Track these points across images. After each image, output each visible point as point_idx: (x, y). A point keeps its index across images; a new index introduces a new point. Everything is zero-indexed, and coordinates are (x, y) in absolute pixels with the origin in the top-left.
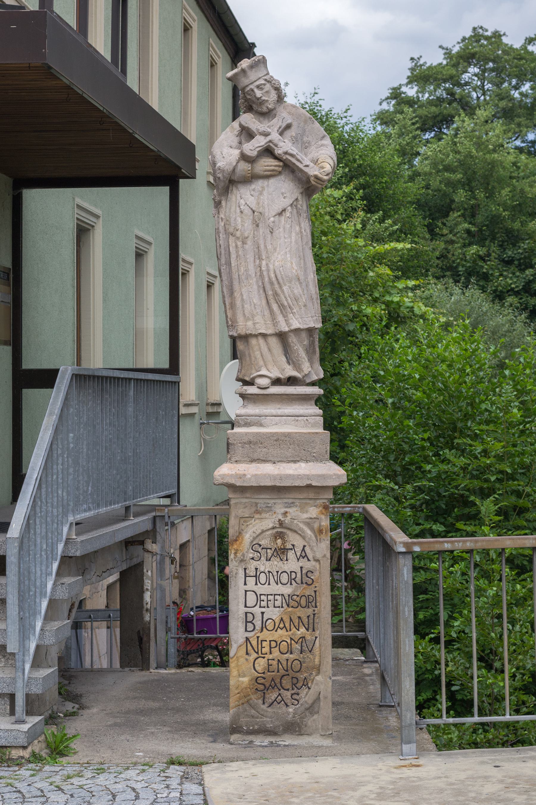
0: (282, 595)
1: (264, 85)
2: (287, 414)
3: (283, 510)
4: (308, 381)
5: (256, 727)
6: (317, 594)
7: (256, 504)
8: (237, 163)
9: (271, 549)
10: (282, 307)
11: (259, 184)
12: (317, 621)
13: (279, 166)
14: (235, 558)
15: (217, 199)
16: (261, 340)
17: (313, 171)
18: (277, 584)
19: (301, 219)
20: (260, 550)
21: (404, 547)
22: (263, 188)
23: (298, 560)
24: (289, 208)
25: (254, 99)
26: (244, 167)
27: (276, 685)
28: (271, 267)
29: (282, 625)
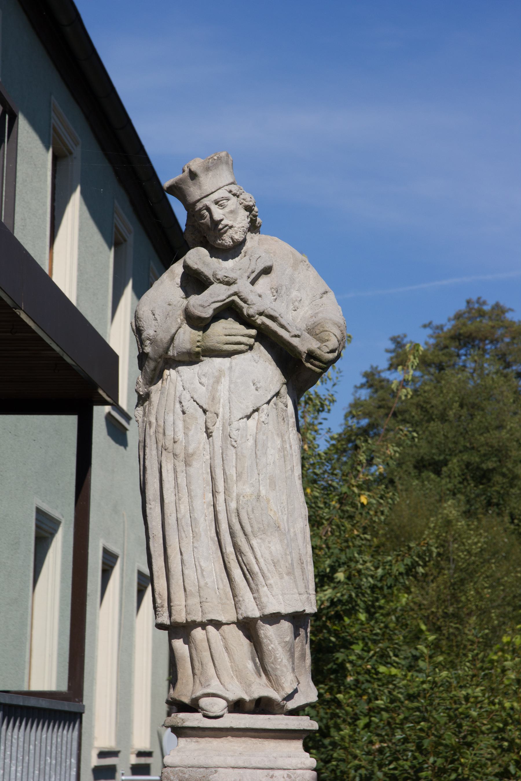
2: (254, 765)
4: (291, 705)
13: (250, 336)
26: (187, 338)
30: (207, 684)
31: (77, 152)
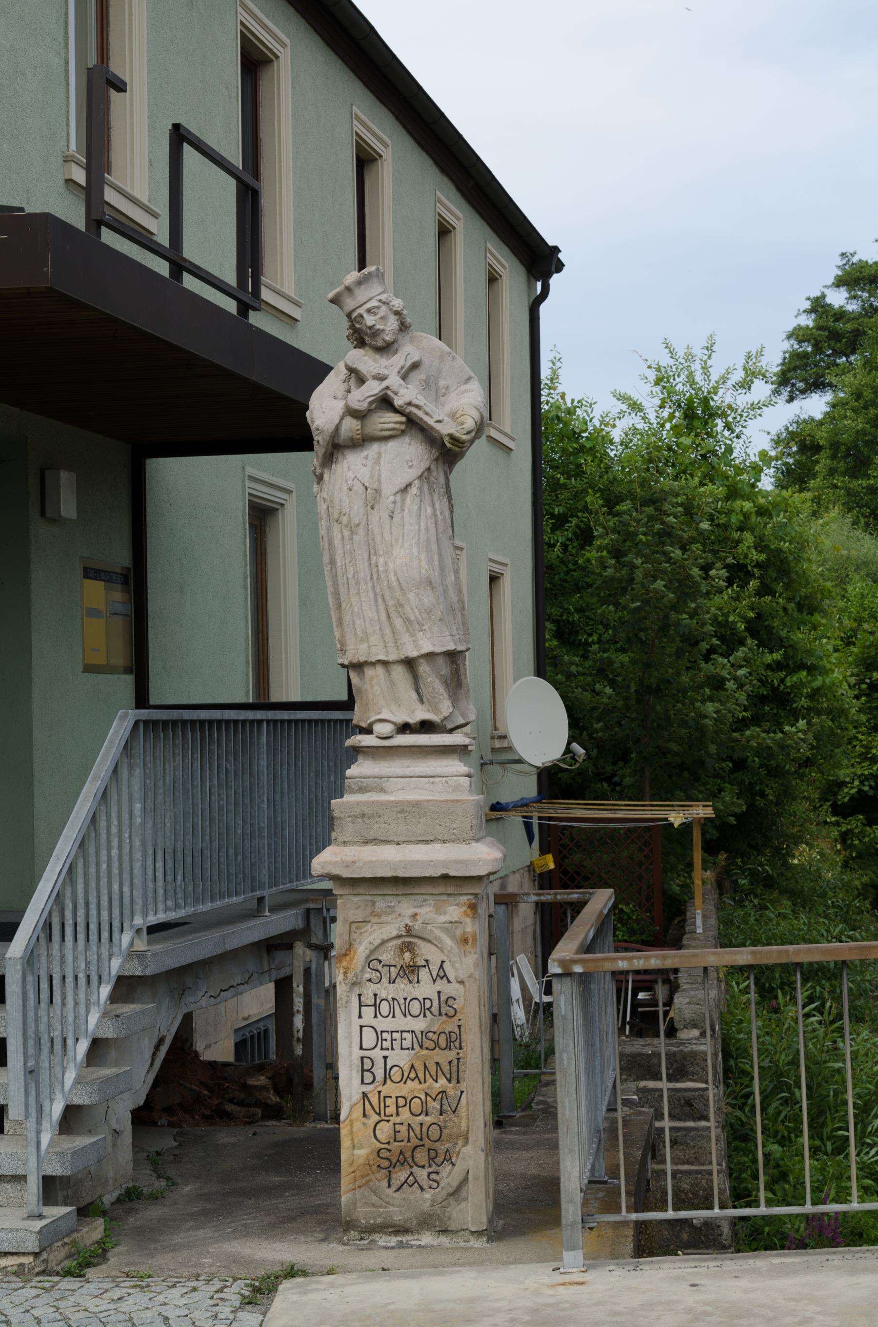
0: (413, 1031)
1: (378, 307)
2: (418, 774)
3: (411, 911)
4: (450, 726)
5: (379, 1220)
6: (462, 1030)
7: (374, 903)
8: (342, 419)
9: (395, 966)
10: (407, 621)
12: (462, 1068)
13: (401, 423)
14: (344, 980)
15: (318, 471)
16: (380, 670)
17: (446, 429)
18: (405, 1015)
20: (380, 968)
21: (559, 966)
22: (380, 453)
23: (434, 981)
24: (416, 482)
25: (364, 328)
26: (351, 425)
27: (405, 1160)
28: (391, 566)
29: (413, 1075)
31: (387, 154)
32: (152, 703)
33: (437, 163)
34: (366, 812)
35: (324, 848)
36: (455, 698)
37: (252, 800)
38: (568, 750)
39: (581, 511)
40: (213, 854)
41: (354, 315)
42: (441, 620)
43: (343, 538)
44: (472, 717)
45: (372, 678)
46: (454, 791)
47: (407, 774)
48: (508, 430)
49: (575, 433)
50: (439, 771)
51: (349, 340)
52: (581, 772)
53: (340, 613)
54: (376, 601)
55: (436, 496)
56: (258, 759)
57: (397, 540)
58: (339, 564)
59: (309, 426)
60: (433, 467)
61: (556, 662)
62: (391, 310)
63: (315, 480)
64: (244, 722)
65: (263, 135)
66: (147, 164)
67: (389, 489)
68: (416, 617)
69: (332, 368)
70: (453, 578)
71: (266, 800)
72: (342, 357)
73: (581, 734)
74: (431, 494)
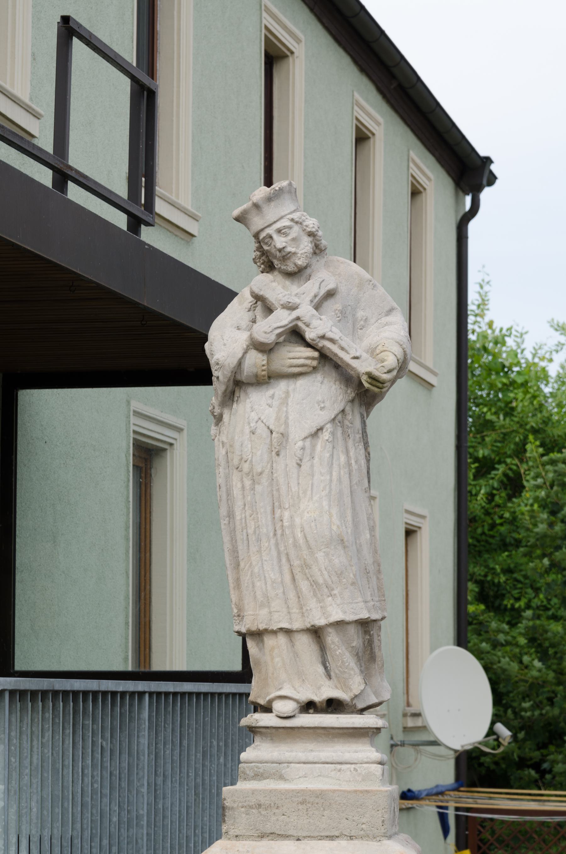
1: (290, 228)
2: (323, 760)
4: (360, 706)
8: (245, 353)
10: (314, 584)
11: (281, 387)
13: (313, 359)
15: (217, 411)
16: (282, 639)
17: (364, 367)
19: (350, 443)
24: (329, 426)
25: (273, 251)
26: (255, 361)
28: (298, 520)
30: (280, 687)
32: (19, 666)
33: (355, 61)
34: (262, 802)
35: (210, 844)
36: (367, 675)
37: (130, 783)
38: (491, 732)
39: (510, 456)
40: (85, 844)
41: (262, 235)
42: (353, 584)
43: (243, 487)
44: (386, 696)
45: (272, 649)
46: (363, 780)
47: (311, 759)
48: (430, 364)
49: (504, 366)
50: (347, 756)
51: (255, 263)
52: (506, 757)
53: (238, 573)
54: (280, 561)
55: (350, 443)
56: (138, 737)
57: (305, 492)
58: (238, 518)
59: (207, 360)
60: (348, 409)
61: (481, 629)
62: (304, 230)
63: (212, 420)
64: (123, 694)
65: (160, 27)
66: (30, 58)
67: (298, 432)
68: (325, 580)
69: (236, 294)
70: (368, 536)
71: (146, 784)
72: (248, 282)
73: (505, 712)
74: (345, 440)
